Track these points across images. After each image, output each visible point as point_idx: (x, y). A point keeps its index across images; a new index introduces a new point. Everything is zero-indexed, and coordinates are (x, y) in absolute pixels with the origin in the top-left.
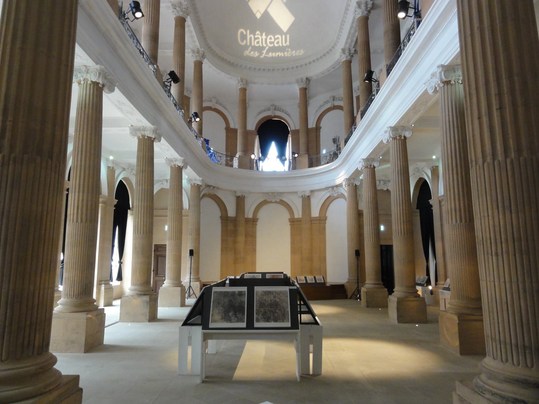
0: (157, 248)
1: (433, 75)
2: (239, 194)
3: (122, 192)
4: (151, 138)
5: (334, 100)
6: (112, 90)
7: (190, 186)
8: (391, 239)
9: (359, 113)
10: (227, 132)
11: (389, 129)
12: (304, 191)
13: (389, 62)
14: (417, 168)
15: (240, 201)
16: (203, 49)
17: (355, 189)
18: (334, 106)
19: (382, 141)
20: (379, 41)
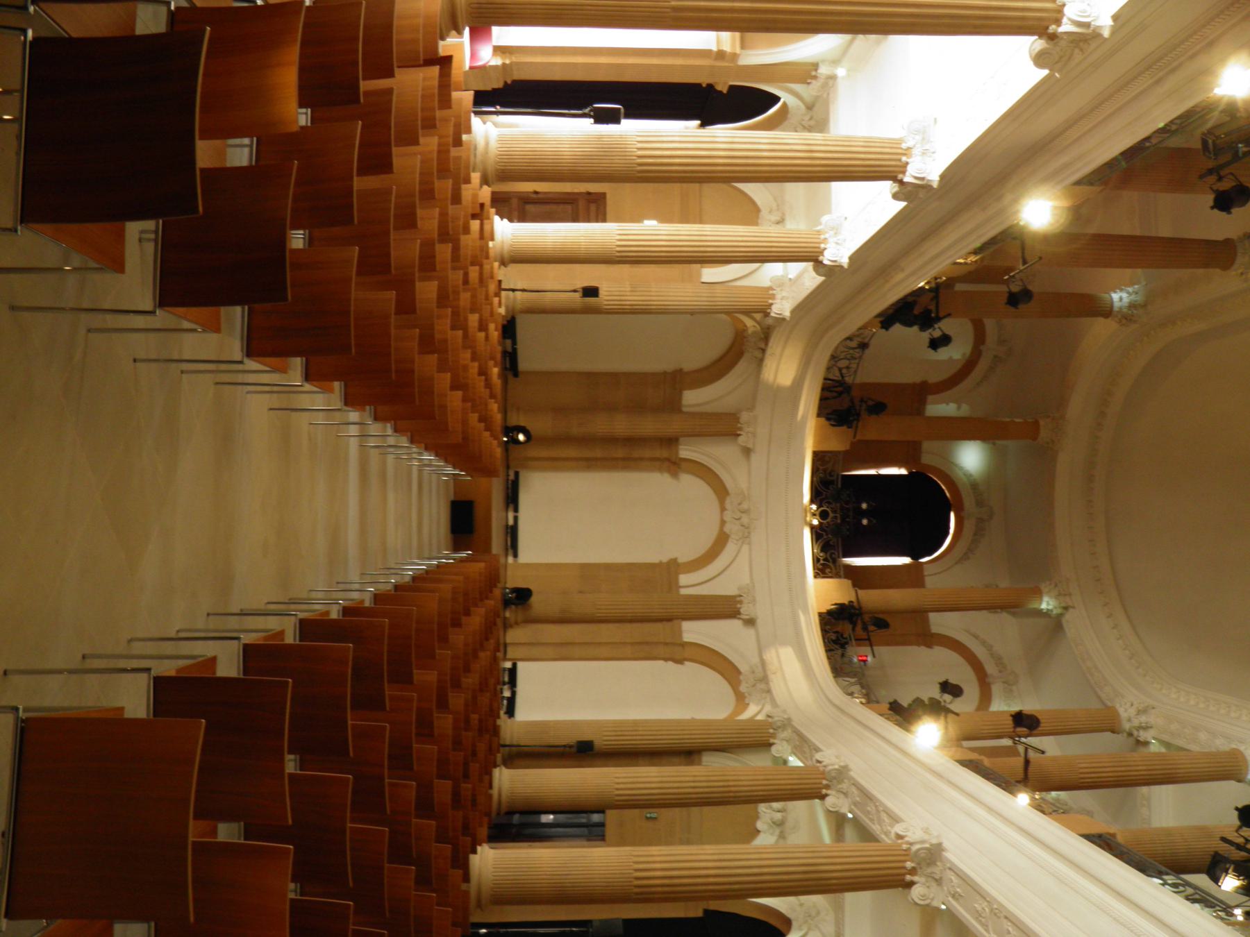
0: (594, 201)
2: (744, 416)
3: (745, 103)
4: (904, 173)
6: (1040, 59)
7: (767, 284)
8: (622, 842)
9: (974, 756)
10: (914, 386)
11: (934, 841)
12: (754, 601)
13: (1120, 839)
14: (818, 913)
15: (725, 426)
17: (756, 740)
20: (1168, 811)
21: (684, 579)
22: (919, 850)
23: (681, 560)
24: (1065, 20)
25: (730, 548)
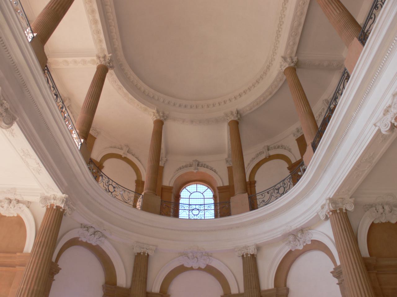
1: (323, 207)
5: (268, 150)
11: (328, 201)
12: (246, 247)
16: (110, 55)
18: (269, 156)
19: (379, 130)
21: (234, 290)
22: (332, 206)
23: (287, 166)
24: (60, 206)
25: (215, 264)
